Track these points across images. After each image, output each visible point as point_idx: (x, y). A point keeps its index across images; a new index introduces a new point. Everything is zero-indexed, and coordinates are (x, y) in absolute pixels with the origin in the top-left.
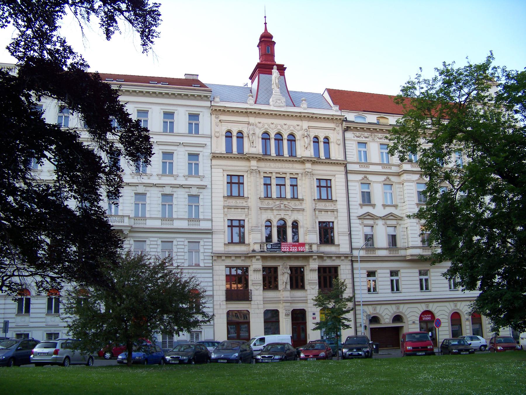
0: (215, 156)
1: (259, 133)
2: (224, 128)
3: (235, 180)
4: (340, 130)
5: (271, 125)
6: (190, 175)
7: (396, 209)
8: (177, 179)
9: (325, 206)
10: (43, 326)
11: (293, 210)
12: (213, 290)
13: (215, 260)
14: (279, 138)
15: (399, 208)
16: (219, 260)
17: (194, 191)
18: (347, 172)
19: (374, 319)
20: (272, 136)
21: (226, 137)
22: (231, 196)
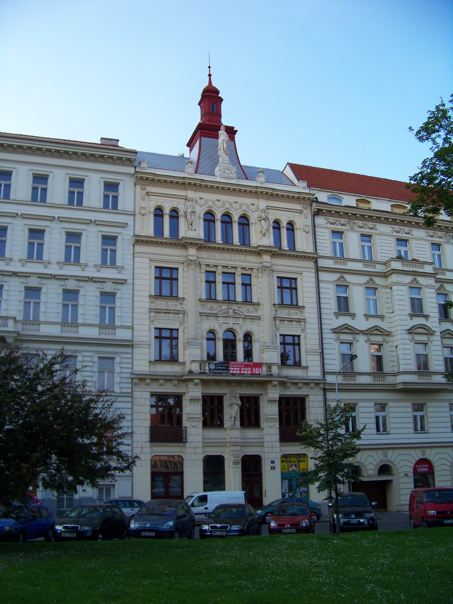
13: (136, 384)
15: (386, 320)
17: (109, 287)
21: (155, 215)
22: (159, 296)
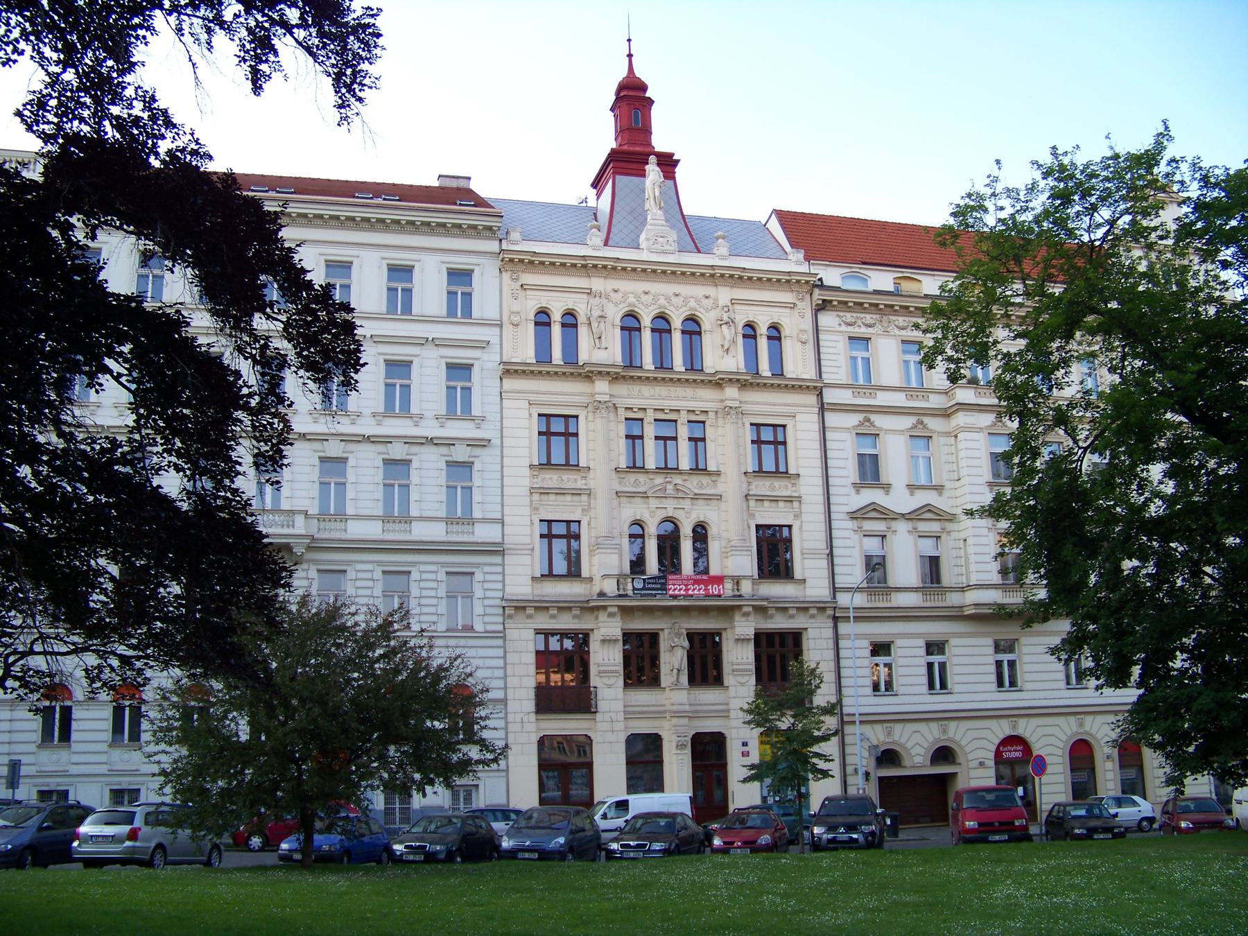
0: (510, 371)
1: (615, 314)
2: (532, 303)
3: (557, 426)
4: (806, 307)
5: (642, 296)
6: (451, 414)
7: (940, 494)
8: (421, 424)
9: (772, 488)
10: (101, 772)
11: (696, 498)
12: (505, 688)
13: (510, 617)
14: (662, 326)
15: (946, 494)
16: (520, 617)
17: (460, 453)
18: (822, 409)
19: (888, 757)
20: (646, 322)
22: (547, 465)
